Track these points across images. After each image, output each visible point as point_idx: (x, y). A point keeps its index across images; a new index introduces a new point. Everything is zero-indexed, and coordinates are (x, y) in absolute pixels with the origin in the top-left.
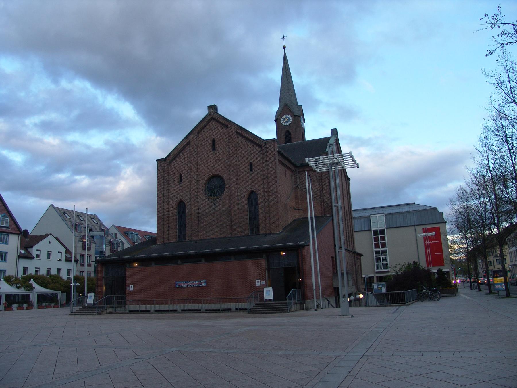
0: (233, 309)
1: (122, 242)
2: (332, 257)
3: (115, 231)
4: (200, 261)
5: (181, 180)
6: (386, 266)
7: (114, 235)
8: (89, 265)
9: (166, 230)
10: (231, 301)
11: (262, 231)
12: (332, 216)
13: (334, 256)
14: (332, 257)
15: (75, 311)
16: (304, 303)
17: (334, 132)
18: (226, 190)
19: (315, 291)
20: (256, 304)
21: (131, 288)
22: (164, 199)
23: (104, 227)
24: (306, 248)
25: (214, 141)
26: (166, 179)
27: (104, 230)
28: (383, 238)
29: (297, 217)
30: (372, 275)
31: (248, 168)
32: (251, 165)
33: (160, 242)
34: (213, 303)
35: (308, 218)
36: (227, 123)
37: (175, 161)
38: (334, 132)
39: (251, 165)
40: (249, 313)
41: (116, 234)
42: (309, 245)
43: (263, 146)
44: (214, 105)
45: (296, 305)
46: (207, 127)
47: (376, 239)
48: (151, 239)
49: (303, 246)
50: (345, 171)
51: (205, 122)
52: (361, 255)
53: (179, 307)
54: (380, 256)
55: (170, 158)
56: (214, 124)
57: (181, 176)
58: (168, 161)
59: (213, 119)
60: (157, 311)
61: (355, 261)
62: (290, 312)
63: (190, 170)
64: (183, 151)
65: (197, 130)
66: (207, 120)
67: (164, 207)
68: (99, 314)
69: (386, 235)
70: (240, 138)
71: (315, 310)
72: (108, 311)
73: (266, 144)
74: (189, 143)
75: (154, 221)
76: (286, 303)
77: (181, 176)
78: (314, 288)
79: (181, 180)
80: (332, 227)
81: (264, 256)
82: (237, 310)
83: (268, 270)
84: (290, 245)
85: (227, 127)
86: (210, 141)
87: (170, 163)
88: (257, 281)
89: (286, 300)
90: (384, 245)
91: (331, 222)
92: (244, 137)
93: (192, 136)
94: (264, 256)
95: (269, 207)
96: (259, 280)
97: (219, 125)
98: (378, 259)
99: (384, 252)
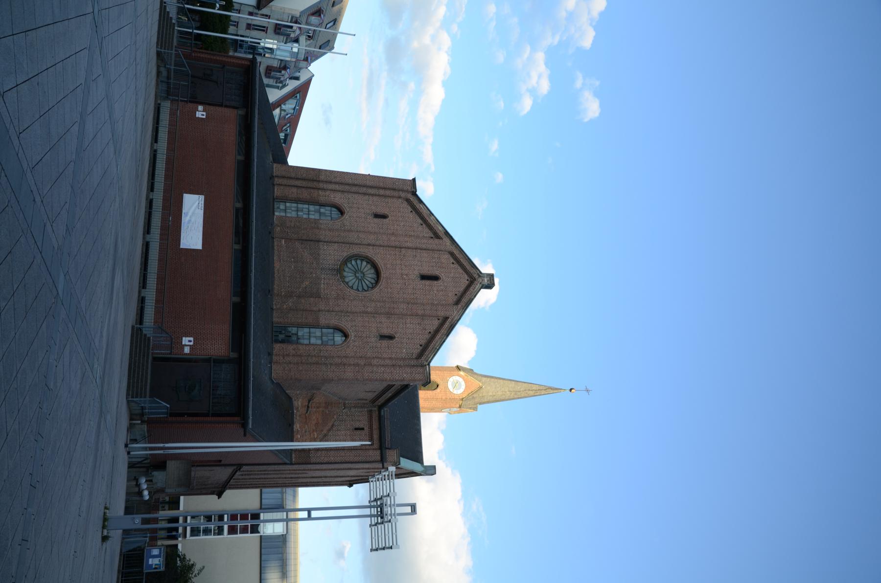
0: (148, 237)
1: (284, 86)
2: (220, 461)
3: (303, 78)
5: (377, 216)
6: (195, 532)
7: (297, 74)
8: (249, 26)
9: (298, 183)
11: (277, 347)
12: (291, 464)
13: (222, 463)
15: (168, 10)
16: (143, 422)
17: (431, 471)
20: (149, 339)
21: (200, 114)
22: (348, 184)
23: (312, 61)
25: (436, 278)
26: (382, 192)
27: (309, 58)
28: (244, 530)
29: (295, 403)
30: (181, 508)
31: (386, 332)
32: (391, 338)
33: (277, 168)
35: (292, 441)
36: (462, 304)
37: (410, 209)
38: (431, 471)
39: (391, 338)
40: (133, 327)
41: (297, 78)
44: (494, 285)
46: (460, 270)
47: (244, 517)
48: (281, 157)
49: (244, 425)
50: (366, 480)
51: (468, 267)
52: (220, 496)
53: (151, 295)
54: (214, 523)
55: (415, 202)
56: (464, 281)
57: (384, 217)
58: (412, 198)
62: (128, 402)
63: (393, 234)
64: (424, 226)
65: (456, 252)
66: (472, 271)
67: (335, 183)
68: (159, 54)
69: (249, 535)
70: (436, 323)
72: (162, 69)
73: (423, 366)
74: (437, 236)
77: (384, 217)
78: (167, 445)
79: (377, 216)
81: (234, 355)
83: (208, 360)
85: (457, 303)
86: (436, 272)
87: (408, 200)
88: (192, 339)
90: (232, 530)
91: (280, 461)
92: (437, 331)
94: (234, 355)
95: (317, 363)
96: (192, 343)
97: (462, 289)
98: (209, 518)
99: (220, 531)
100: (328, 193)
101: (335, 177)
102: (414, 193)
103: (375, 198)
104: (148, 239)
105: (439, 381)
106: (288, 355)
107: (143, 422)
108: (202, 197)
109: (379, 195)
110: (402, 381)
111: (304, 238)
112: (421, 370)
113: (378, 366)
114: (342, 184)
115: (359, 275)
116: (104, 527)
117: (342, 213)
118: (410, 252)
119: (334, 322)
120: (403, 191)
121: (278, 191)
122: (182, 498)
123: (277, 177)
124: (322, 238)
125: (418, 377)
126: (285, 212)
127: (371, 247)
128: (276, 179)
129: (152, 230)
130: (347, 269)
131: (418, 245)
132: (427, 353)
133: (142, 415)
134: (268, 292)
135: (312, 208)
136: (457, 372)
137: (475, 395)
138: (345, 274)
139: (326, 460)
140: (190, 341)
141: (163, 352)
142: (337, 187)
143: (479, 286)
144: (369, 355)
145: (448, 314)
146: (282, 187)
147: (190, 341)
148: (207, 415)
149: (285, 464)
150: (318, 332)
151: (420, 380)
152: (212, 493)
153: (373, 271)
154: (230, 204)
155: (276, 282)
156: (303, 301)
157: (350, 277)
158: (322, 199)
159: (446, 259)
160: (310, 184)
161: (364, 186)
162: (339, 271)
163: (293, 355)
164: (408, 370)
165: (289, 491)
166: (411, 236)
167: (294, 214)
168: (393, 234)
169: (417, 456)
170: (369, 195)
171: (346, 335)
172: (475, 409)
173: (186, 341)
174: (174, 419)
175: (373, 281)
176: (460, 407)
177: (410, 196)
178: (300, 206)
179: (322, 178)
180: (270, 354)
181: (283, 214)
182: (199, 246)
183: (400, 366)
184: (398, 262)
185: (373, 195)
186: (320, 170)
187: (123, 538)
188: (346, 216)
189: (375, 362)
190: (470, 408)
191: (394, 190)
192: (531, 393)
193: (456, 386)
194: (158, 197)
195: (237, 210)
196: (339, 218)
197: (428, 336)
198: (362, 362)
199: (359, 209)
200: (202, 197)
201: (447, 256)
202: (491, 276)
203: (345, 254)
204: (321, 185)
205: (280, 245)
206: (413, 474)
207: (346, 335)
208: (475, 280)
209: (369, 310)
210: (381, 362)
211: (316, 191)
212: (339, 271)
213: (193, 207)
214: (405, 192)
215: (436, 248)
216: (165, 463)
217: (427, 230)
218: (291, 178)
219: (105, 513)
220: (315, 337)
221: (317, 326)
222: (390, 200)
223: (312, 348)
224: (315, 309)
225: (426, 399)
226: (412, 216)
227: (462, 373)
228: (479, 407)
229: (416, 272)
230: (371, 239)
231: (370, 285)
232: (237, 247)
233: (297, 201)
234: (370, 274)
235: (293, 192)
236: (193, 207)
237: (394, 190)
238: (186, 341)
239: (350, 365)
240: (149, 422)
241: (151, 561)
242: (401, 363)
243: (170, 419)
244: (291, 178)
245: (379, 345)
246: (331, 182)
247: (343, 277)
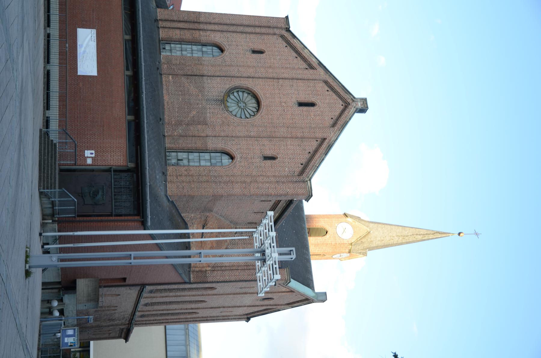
0: (48, 113)
2: (124, 279)
4: (127, 69)
5: (254, 52)
10: (62, 114)
12: (190, 283)
13: (127, 282)
14: (124, 279)
16: (54, 221)
17: (322, 298)
19: (71, 233)
20: (55, 144)
24: (142, 227)
25: (312, 105)
26: (258, 30)
31: (269, 153)
32: (273, 158)
34: (60, 81)
37: (285, 44)
38: (322, 298)
39: (273, 158)
40: (41, 130)
42: (145, 229)
43: (302, 177)
45: (50, 206)
46: (335, 96)
51: (342, 93)
52: (126, 339)
53: (54, 113)
55: (290, 38)
57: (261, 52)
58: (286, 34)
59: (347, 105)
60: (48, 75)
61: (117, 325)
63: (270, 67)
65: (330, 81)
66: (346, 96)
67: (214, 24)
70: (315, 144)
71: (40, 234)
73: (304, 182)
74: (311, 67)
76: (55, 189)
77: (261, 52)
79: (254, 52)
80: (173, 281)
82: (49, 36)
84: (146, 204)
85: (334, 125)
87: (282, 36)
88: (93, 152)
89: (60, 188)
92: (316, 151)
94: (131, 165)
95: (208, 181)
96: (93, 156)
97: (337, 113)
100: (208, 33)
101: (214, 18)
102: (288, 30)
103: (252, 36)
104: (48, 67)
105: (327, 228)
106: (181, 176)
107: (54, 221)
108: (94, 31)
109: (255, 33)
110: (285, 195)
111: (189, 73)
112: (303, 185)
113: (263, 183)
114: (221, 24)
115: (242, 105)
116: (26, 262)
117: (222, 50)
118: (287, 82)
119: (220, 145)
120: (277, 28)
121: (163, 34)
122: (92, 343)
123: (161, 20)
124: (205, 73)
125: (300, 191)
126: (172, 53)
127: (251, 80)
128: (160, 23)
129: (52, 24)
130: (230, 100)
131: (295, 76)
132: (307, 170)
133: (53, 215)
134: (159, 120)
135: (194, 48)
136: (345, 219)
137: (363, 240)
138: (229, 104)
139: (222, 279)
140: (92, 154)
141: (68, 163)
142: (216, 27)
143: (353, 110)
144: (254, 173)
145: (325, 135)
146: (166, 30)
147: (92, 154)
148: (111, 215)
149: (185, 283)
150: (207, 156)
151: (303, 194)
152: (120, 337)
153: (254, 101)
154: (119, 37)
155: (166, 113)
156: (192, 128)
157: (232, 106)
158: (204, 39)
159: (321, 86)
160: (191, 26)
161: (241, 25)
162: (223, 101)
163: (186, 176)
164: (291, 185)
165: (191, 325)
166: (287, 68)
167: (179, 53)
168: (270, 67)
169: (308, 282)
170: (246, 33)
171: (232, 158)
172: (365, 254)
173: (88, 153)
174: (81, 219)
175: (255, 110)
176: (349, 252)
177: (284, 33)
178: (184, 46)
179: (202, 19)
180: (164, 174)
181: (169, 54)
182: (94, 73)
183: (283, 182)
184: (277, 91)
185: (250, 33)
186: (199, 12)
187: (41, 321)
188: (226, 53)
189: (260, 179)
190: (360, 253)
191: (269, 27)
192: (419, 237)
193: (345, 232)
194: (55, 31)
195: (129, 122)
196: (220, 55)
197: (308, 156)
198: (248, 180)
199: (238, 46)
200: (94, 31)
201: (322, 84)
202: (365, 101)
203: (227, 86)
204: (202, 26)
205: (168, 81)
206: (307, 301)
207: (232, 158)
208: (348, 105)
209: (252, 134)
210: (265, 179)
211: (197, 32)
212: (223, 101)
213: (87, 40)
214: (280, 29)
215: (311, 77)
216: (74, 282)
217: (302, 62)
218: (174, 21)
219: (26, 251)
220: (205, 160)
221: (205, 151)
222: (265, 37)
223: (202, 169)
224: (202, 135)
225: (317, 245)
226: (288, 51)
227: (349, 219)
228: (369, 253)
229: (294, 100)
230: (251, 72)
231: (252, 114)
232: (131, 118)
233: (181, 42)
234: (252, 104)
235: (176, 34)
236: (87, 40)
237: (269, 27)
238: (88, 153)
239: (237, 182)
240: (59, 222)
241: (66, 340)
242: (284, 180)
243: (78, 219)
244: (174, 21)
245: (263, 165)
246: (210, 23)
247: (226, 108)
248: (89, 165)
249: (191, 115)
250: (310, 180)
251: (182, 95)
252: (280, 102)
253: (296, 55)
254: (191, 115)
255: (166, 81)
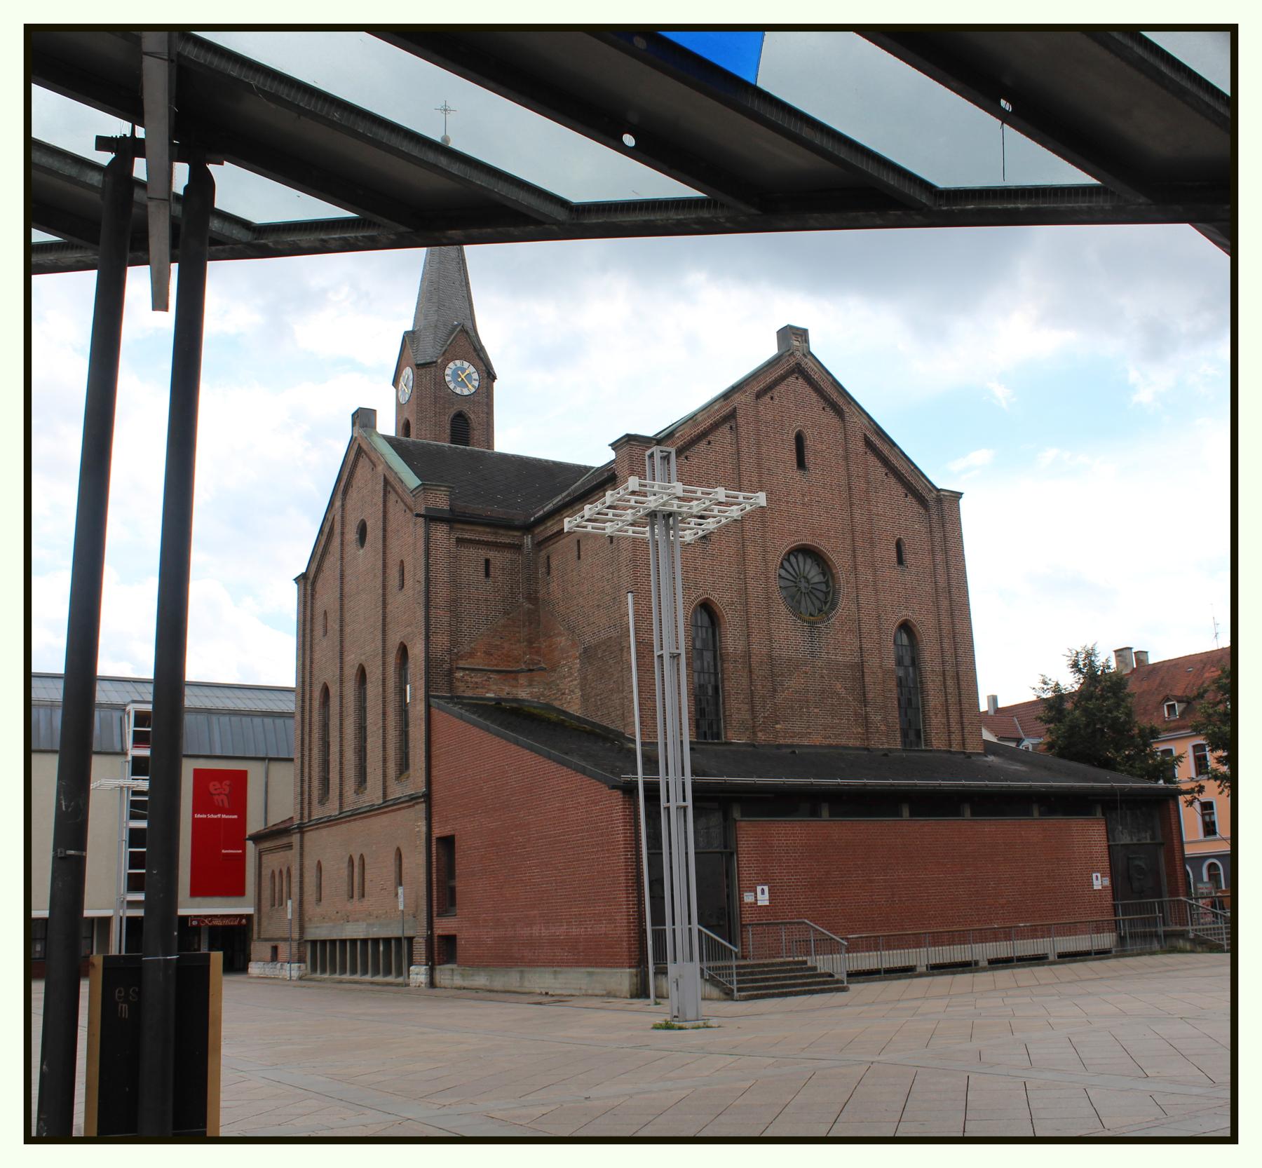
10: (983, 937)
18: (842, 602)
25: (799, 439)
70: (872, 460)
74: (732, 415)
75: (61, 692)
76: (730, 968)
85: (839, 412)
88: (759, 888)
92: (885, 462)
93: (738, 399)
96: (766, 888)
97: (814, 395)
104: (984, 963)
145: (859, 435)
155: (844, 742)
197: (893, 480)
232: (825, 812)
248: (741, 899)
249: (843, 692)
250: (939, 490)
251: (808, 708)
252: (804, 504)
253: (704, 442)
254: (843, 692)
255: (785, 738)
